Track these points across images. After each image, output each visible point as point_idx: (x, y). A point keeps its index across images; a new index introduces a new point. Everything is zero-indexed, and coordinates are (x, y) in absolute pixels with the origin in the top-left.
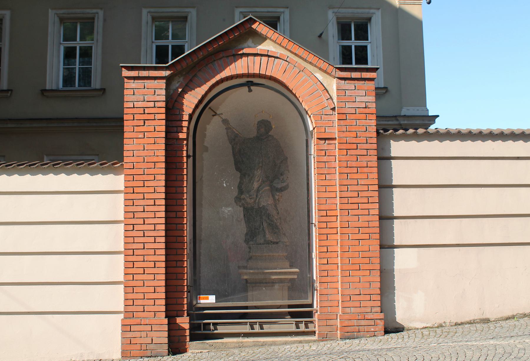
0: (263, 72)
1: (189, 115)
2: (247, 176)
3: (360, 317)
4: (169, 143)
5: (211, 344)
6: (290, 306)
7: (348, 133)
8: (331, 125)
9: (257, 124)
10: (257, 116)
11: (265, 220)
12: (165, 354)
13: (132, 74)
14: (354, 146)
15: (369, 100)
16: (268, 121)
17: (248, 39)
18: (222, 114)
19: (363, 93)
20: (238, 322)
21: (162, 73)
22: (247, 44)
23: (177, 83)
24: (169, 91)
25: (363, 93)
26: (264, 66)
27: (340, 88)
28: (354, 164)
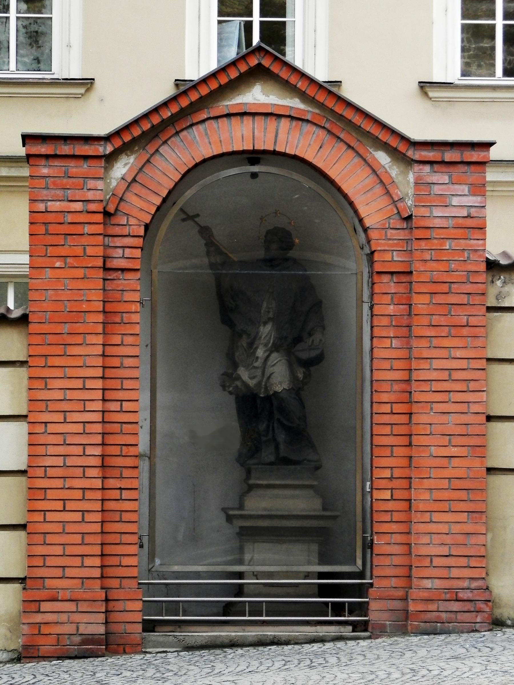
0: (280, 148)
1: (144, 225)
2: (244, 336)
3: (448, 596)
4: (109, 278)
5: (181, 637)
6: (321, 575)
7: (434, 265)
8: (403, 247)
9: (265, 236)
10: (266, 220)
11: (279, 420)
12: (403, 301)
13: (43, 150)
14: (445, 288)
15: (474, 203)
16: (283, 230)
17: (255, 85)
18: (198, 215)
19: (463, 190)
20: (216, 628)
21: (98, 150)
22: (251, 94)
23: (124, 167)
24: (108, 181)
25: (463, 190)
26: (282, 136)
27: (420, 180)
28: (443, 321)
